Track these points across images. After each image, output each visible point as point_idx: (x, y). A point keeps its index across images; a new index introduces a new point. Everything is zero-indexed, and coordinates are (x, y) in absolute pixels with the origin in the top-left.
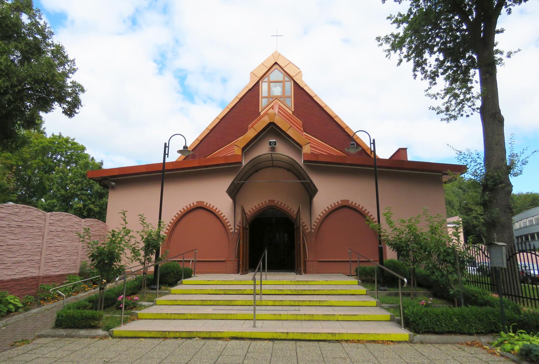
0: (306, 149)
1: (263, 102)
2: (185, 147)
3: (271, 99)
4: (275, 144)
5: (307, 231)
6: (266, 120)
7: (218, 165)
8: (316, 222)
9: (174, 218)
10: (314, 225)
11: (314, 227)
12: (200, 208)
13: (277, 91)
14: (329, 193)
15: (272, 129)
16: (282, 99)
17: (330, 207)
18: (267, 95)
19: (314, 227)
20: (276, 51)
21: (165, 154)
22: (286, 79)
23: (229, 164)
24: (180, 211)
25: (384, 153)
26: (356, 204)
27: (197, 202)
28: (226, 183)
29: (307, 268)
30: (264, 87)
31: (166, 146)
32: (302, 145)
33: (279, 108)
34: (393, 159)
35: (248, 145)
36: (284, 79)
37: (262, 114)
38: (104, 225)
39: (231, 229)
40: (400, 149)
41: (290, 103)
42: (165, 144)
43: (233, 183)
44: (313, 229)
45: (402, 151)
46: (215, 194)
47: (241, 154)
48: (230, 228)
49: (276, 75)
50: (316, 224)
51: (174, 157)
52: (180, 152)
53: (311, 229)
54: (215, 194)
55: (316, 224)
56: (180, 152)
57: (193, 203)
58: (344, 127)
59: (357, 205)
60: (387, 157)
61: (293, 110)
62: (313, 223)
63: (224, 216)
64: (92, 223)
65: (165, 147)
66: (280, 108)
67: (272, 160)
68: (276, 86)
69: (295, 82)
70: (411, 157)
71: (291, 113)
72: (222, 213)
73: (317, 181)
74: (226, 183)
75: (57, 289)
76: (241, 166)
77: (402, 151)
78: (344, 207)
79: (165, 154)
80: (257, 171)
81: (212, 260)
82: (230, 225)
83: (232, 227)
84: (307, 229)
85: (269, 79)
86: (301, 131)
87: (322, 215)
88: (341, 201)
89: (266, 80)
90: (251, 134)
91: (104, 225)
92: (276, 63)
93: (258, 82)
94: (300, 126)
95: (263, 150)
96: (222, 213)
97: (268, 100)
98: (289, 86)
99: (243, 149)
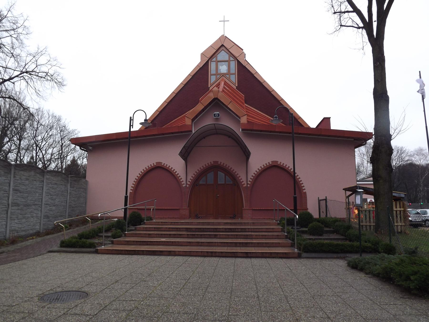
0: (244, 120)
1: (212, 79)
2: (146, 120)
3: (218, 76)
4: (219, 116)
5: (244, 186)
6: (211, 96)
7: (172, 133)
8: (251, 178)
9: (284, 165)
10: (250, 181)
11: (250, 183)
12: (159, 168)
13: (223, 69)
14: (261, 155)
15: (216, 103)
16: (228, 76)
17: (260, 169)
18: (215, 73)
19: (250, 183)
20: (223, 36)
21: (130, 126)
22: (232, 59)
23: (182, 132)
24: (141, 172)
25: (313, 122)
26: (283, 164)
27: (214, 162)
28: (178, 147)
29: (344, 206)
30: (212, 66)
31: (131, 120)
32: (240, 116)
33: (225, 84)
34: (319, 128)
35: (196, 116)
36: (229, 58)
37: (210, 89)
38: (84, 181)
39: (184, 184)
40: (324, 118)
41: (234, 79)
42: (131, 118)
43: (184, 147)
44: (249, 184)
45: (326, 121)
46: (171, 157)
47: (190, 124)
48: (182, 183)
49: (223, 55)
50: (251, 180)
51: (137, 127)
52: (141, 124)
53: (247, 184)
54: (171, 157)
55: (251, 180)
56: (141, 124)
57: (153, 164)
58: (279, 99)
59: (284, 165)
60: (311, 127)
61: (237, 85)
62: (249, 179)
63: (178, 174)
64: (76, 179)
65: (131, 120)
66: (226, 84)
67: (216, 129)
68: (222, 65)
69: (238, 62)
70: (334, 126)
71: (235, 88)
72: (176, 172)
73: (252, 146)
74: (178, 147)
75: (59, 222)
76: (191, 134)
77: (326, 121)
78: (275, 167)
79: (131, 126)
80: (204, 138)
81: (165, 208)
82: (183, 181)
83: (184, 182)
84: (244, 184)
85: (217, 59)
86: (243, 103)
87: (256, 173)
88: (272, 162)
89: (214, 59)
90: (199, 107)
91: (84, 181)
92: (222, 45)
93: (207, 62)
94: (243, 99)
95: (208, 121)
96: (176, 172)
97: (216, 77)
98: (233, 65)
99: (193, 120)
